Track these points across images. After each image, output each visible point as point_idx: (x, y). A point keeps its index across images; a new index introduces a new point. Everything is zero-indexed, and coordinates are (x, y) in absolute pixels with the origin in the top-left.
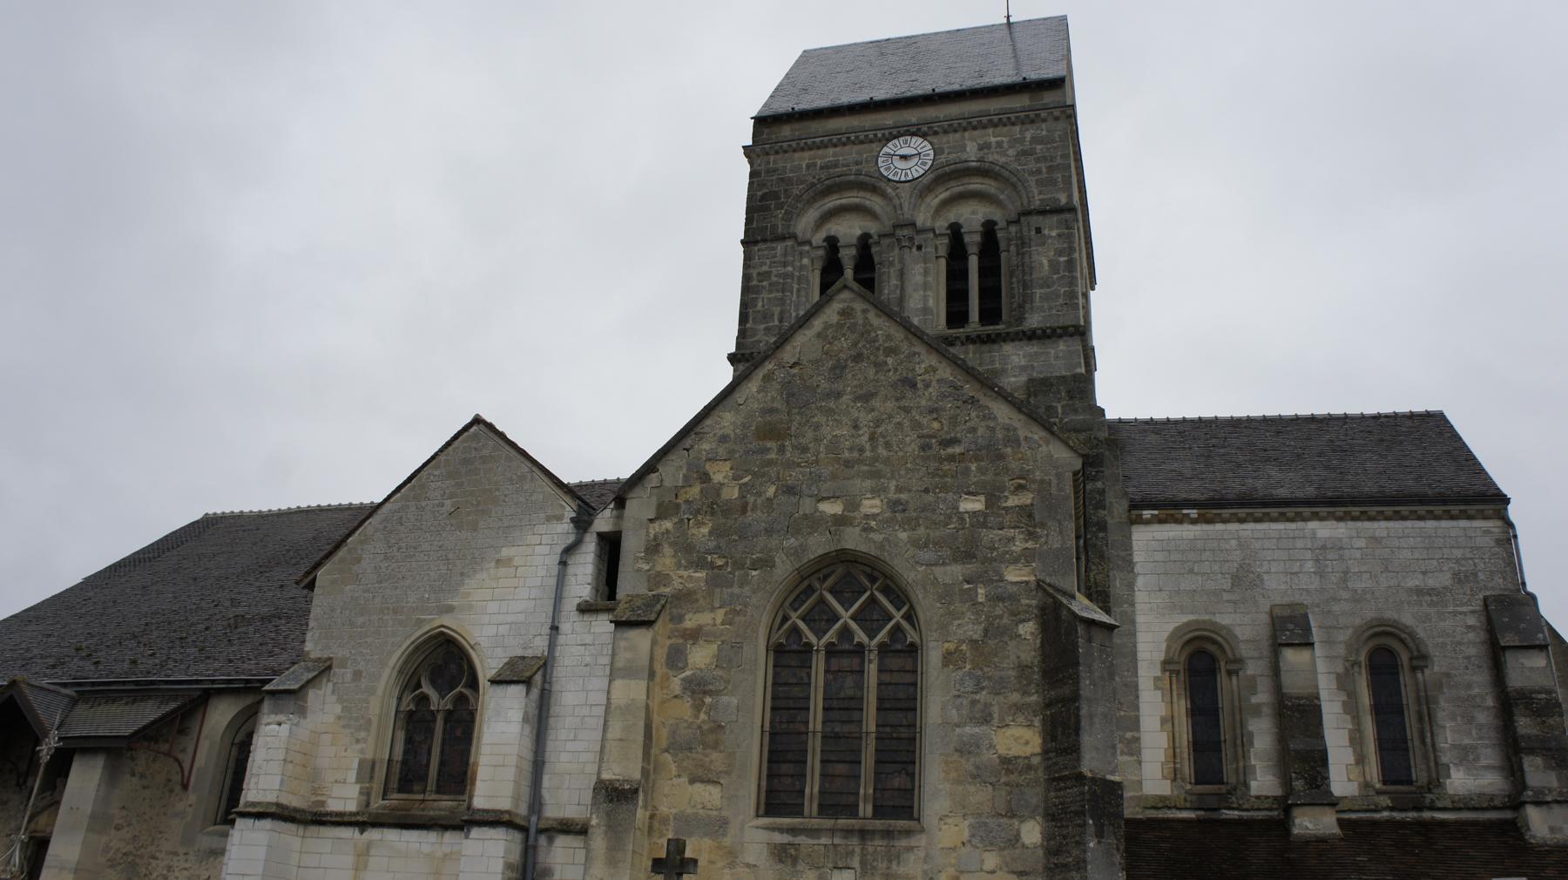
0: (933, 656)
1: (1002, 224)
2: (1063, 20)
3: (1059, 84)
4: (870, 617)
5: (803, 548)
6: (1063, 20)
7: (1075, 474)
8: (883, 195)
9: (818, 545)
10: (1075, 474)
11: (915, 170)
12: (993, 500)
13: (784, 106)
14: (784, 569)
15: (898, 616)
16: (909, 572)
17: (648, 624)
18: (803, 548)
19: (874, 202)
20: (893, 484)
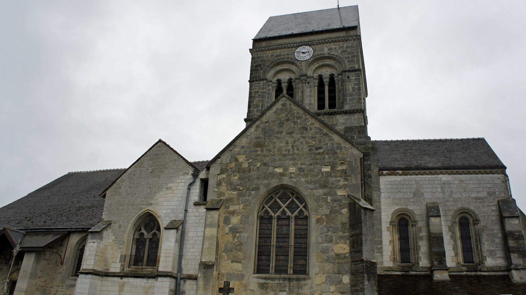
0: (313, 220)
1: (336, 75)
4: (292, 207)
5: (269, 184)
7: (361, 159)
8: (296, 65)
9: (275, 183)
10: (361, 159)
11: (307, 57)
14: (263, 191)
17: (217, 209)
19: (293, 68)
20: (299, 162)
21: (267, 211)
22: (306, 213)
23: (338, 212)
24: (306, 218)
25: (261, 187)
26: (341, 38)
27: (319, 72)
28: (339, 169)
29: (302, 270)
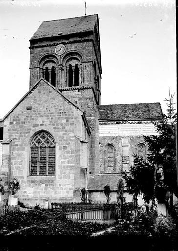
0: (57, 148)
1: (79, 65)
2: (30, 40)
3: (96, 32)
4: (47, 141)
5: (35, 130)
6: (30, 40)
7: (82, 116)
8: (56, 58)
9: (38, 129)
10: (82, 116)
11: (61, 52)
12: (67, 121)
13: (41, 35)
14: (32, 133)
15: (52, 141)
16: (52, 132)
17: (9, 144)
18: (35, 130)
19: (55, 60)
20: (50, 118)
21: (35, 144)
22: (54, 145)
23: (116, 182)
24: (54, 147)
25: (31, 131)
26: (86, 35)
27: (70, 62)
28: (155, 165)
29: (52, 173)
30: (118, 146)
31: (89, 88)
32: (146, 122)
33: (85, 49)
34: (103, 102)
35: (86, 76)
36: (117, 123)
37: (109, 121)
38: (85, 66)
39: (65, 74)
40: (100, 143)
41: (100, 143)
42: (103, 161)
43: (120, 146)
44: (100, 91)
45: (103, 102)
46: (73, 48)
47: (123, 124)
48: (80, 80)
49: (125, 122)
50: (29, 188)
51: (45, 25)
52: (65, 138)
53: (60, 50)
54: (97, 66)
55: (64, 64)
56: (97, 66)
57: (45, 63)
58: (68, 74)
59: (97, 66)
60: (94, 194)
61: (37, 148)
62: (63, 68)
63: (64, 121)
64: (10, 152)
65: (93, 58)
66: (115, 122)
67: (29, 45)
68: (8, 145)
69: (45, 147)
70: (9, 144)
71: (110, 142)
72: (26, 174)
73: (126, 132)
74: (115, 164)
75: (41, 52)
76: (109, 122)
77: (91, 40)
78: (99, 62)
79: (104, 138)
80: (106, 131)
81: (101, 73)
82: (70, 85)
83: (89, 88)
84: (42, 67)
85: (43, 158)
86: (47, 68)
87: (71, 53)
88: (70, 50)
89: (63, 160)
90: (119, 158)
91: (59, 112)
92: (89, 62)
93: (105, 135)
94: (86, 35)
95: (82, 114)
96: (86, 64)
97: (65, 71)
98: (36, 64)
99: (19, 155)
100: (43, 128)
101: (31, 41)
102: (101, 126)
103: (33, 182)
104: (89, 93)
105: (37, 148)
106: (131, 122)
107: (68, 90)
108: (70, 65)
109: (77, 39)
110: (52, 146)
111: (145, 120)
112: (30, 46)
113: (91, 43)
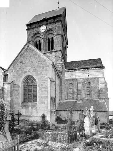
7: (52, 64)
8: (40, 34)
10: (52, 64)
17: (10, 84)
26: (59, 18)
27: (49, 36)
29: (35, 101)
30: (75, 84)
31: (59, 51)
32: (92, 69)
33: (56, 27)
34: (69, 60)
35: (57, 46)
36: (75, 71)
37: (70, 70)
38: (57, 37)
39: (46, 44)
40: (65, 83)
41: (65, 83)
42: (67, 93)
43: (77, 84)
44: (67, 55)
45: (69, 60)
46: (50, 27)
47: (79, 71)
48: (54, 46)
49: (79, 70)
50: (22, 110)
51: (36, 17)
52: (42, 79)
53: (43, 29)
54: (64, 37)
55: (45, 38)
56: (64, 38)
57: (36, 38)
58: (48, 44)
59: (64, 38)
60: (61, 112)
61: (27, 86)
62: (45, 40)
63: (41, 69)
64: (12, 89)
65: (61, 32)
66: (74, 70)
67: (26, 28)
68: (10, 85)
69: (31, 86)
70: (10, 84)
71: (70, 82)
72: (21, 101)
73: (80, 76)
74: (73, 95)
75: (33, 32)
76: (70, 71)
77: (61, 21)
78: (66, 37)
79: (67, 80)
80: (68, 75)
81: (67, 45)
82: (49, 50)
83: (59, 51)
84: (33, 41)
85: (30, 92)
86: (36, 41)
87: (49, 30)
88: (48, 28)
89: (41, 93)
90: (76, 91)
91: (43, 69)
92: (59, 35)
93: (68, 78)
94: (59, 18)
95: (52, 63)
96: (57, 36)
97: (46, 42)
98: (30, 39)
99: (16, 90)
100: (30, 74)
101: (27, 25)
102: (65, 73)
103: (24, 106)
104: (59, 54)
105: (27, 86)
106: (83, 70)
107: (47, 53)
108: (49, 38)
109: (52, 20)
110: (35, 84)
111: (92, 68)
112: (27, 28)
113: (60, 23)
